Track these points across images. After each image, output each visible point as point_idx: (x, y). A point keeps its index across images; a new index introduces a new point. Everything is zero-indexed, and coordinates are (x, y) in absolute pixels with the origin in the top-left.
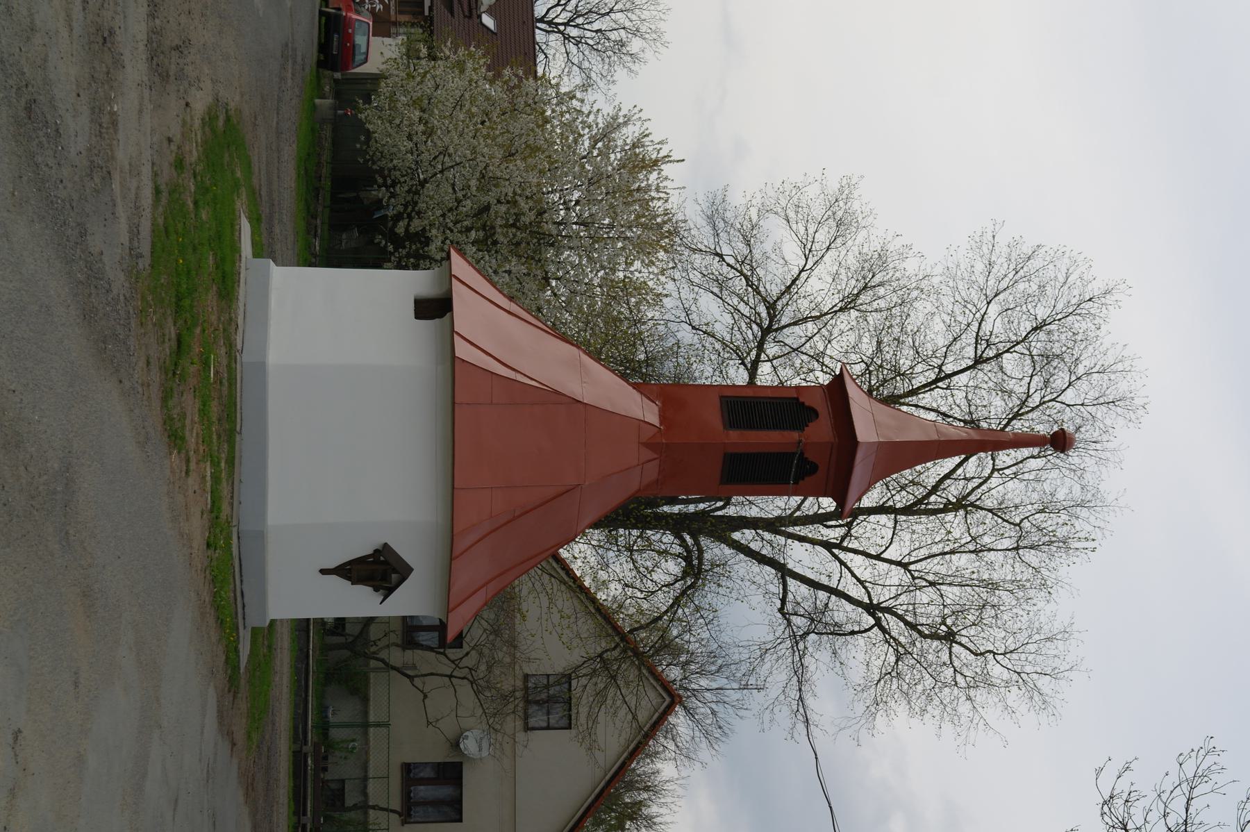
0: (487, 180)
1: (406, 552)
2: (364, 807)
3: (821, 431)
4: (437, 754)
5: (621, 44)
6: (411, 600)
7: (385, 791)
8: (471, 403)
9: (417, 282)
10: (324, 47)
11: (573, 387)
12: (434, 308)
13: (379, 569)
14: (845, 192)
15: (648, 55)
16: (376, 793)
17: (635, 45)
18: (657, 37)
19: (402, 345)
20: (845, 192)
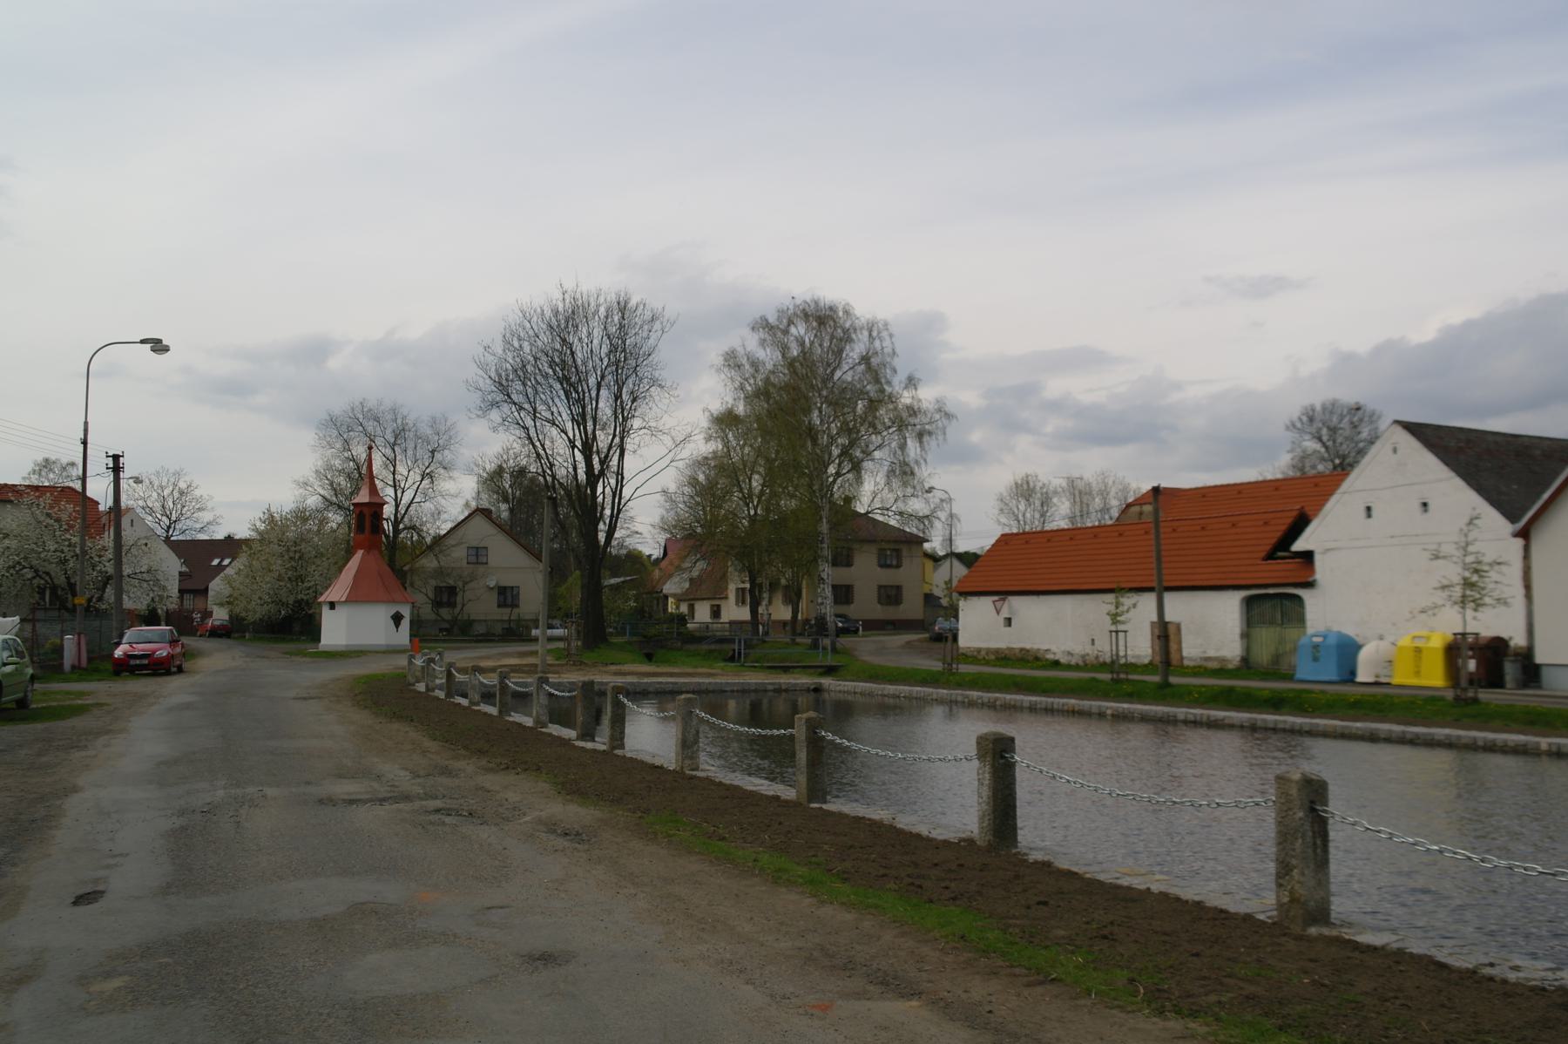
0: (280, 578)
1: (393, 612)
2: (510, 621)
3: (366, 511)
4: (495, 596)
5: (182, 493)
6: (406, 611)
7: (504, 613)
8: (357, 596)
9: (326, 611)
10: (220, 636)
11: (353, 572)
12: (332, 605)
13: (397, 618)
14: (297, 483)
15: (188, 479)
16: (506, 618)
17: (182, 485)
18: (178, 474)
19: (342, 613)
20: (297, 483)
